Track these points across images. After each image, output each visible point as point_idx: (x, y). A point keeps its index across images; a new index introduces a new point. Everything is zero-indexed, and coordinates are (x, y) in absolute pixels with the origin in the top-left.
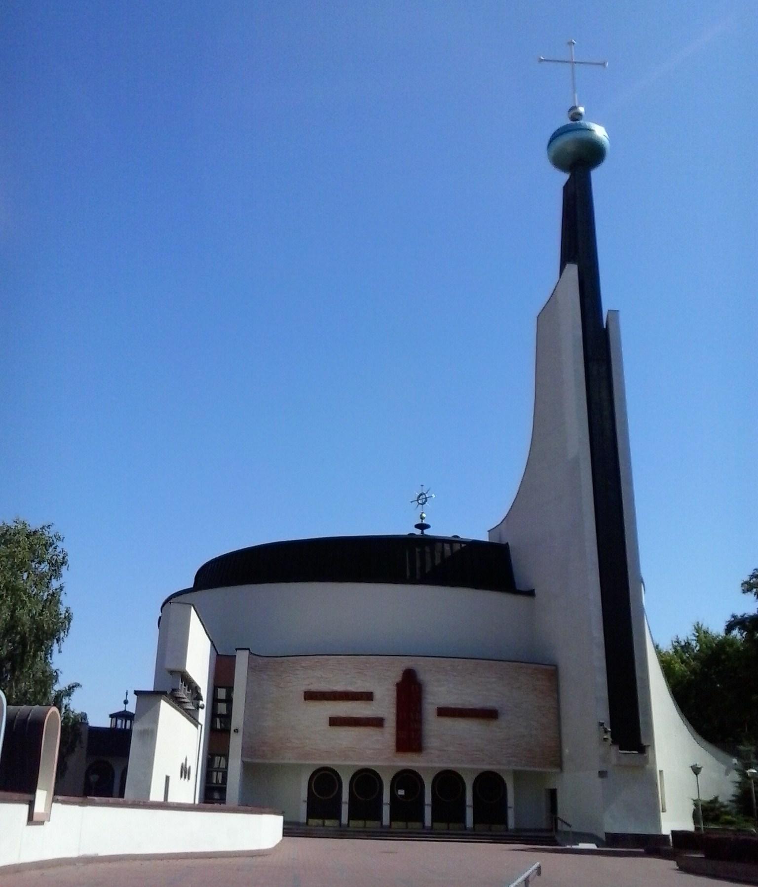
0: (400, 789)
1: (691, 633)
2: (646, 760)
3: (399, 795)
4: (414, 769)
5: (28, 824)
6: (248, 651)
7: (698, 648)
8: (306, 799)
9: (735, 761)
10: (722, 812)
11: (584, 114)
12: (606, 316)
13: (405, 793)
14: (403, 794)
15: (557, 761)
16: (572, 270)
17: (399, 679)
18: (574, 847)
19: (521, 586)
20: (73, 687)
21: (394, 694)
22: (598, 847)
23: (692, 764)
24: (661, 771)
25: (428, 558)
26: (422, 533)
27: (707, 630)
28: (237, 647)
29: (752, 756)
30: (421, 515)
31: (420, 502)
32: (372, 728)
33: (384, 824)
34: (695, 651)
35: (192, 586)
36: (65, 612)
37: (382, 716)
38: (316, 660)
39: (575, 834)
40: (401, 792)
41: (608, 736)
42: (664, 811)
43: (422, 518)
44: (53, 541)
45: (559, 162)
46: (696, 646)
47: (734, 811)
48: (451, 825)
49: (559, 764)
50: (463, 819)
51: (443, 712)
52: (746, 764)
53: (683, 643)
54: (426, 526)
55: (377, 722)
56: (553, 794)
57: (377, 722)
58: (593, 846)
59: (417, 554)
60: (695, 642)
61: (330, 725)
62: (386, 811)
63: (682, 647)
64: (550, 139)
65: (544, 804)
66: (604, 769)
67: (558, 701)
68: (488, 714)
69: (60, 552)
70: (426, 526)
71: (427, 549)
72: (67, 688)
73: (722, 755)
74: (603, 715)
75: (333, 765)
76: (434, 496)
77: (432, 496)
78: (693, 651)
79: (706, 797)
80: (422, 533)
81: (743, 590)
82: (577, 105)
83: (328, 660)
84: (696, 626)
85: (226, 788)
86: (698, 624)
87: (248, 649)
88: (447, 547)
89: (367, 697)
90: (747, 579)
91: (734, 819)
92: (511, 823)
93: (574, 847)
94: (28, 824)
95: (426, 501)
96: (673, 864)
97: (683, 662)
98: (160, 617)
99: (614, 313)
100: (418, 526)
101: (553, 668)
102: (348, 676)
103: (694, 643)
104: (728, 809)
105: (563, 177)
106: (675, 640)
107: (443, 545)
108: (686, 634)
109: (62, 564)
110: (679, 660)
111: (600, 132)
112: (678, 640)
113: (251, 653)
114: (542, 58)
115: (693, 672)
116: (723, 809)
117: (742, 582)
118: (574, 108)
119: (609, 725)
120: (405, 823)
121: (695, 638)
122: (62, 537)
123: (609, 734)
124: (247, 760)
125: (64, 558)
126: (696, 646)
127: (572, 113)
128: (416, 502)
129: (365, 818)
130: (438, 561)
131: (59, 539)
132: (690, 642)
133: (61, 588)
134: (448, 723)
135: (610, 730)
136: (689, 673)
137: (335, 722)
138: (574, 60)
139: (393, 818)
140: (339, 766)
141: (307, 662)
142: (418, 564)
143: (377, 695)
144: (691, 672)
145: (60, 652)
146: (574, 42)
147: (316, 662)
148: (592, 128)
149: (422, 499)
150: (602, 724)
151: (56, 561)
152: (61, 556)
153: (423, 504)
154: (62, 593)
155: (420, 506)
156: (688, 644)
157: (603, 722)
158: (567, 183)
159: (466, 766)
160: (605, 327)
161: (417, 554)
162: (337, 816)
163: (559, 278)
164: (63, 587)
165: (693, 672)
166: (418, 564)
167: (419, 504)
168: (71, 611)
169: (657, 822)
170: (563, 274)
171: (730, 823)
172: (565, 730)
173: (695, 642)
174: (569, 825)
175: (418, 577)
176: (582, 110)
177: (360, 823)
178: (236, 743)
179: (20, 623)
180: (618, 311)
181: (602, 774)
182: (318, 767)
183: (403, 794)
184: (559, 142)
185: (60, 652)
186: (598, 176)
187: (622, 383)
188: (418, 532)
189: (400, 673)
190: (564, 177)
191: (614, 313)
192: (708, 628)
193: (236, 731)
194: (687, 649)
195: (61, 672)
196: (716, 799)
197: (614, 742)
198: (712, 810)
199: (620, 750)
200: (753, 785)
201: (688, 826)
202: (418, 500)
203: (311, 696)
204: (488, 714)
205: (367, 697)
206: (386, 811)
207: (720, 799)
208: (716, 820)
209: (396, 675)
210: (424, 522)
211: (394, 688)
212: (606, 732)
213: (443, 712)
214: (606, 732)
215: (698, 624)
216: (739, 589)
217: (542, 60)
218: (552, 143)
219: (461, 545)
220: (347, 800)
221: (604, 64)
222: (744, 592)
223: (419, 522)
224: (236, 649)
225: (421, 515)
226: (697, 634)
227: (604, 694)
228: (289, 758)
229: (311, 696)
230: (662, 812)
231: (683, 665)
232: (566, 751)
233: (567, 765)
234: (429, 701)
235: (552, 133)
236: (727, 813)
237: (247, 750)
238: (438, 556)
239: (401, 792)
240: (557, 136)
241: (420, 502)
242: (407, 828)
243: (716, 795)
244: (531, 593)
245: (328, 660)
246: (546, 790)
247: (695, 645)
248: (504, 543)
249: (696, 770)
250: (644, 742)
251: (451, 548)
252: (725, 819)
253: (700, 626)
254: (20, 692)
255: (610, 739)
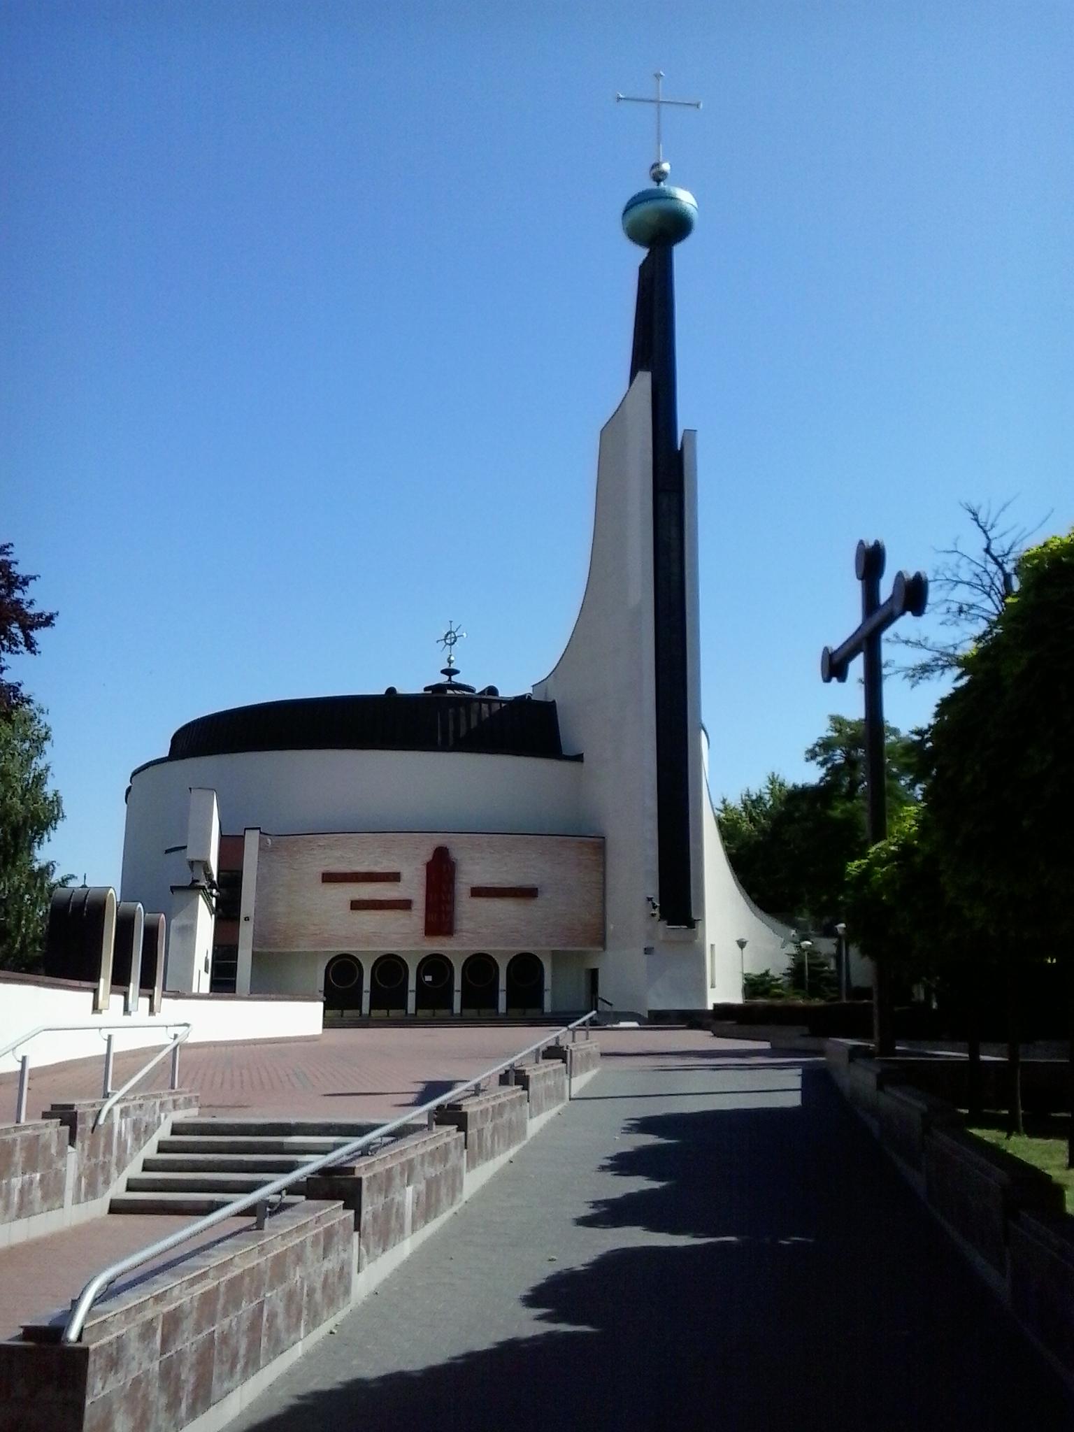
0: (427, 975)
1: (764, 786)
2: (695, 935)
3: (427, 982)
4: (399, 955)
5: (124, 1014)
6: (258, 831)
7: (771, 803)
8: (323, 989)
9: (793, 932)
10: (772, 985)
11: (669, 172)
12: (682, 435)
13: (433, 978)
14: (431, 980)
15: (601, 940)
16: (645, 378)
17: (429, 858)
18: (614, 1026)
19: (566, 751)
20: (67, 879)
21: (424, 873)
22: (640, 1024)
23: (738, 939)
24: (712, 946)
25: (463, 720)
26: (450, 680)
27: (783, 781)
28: (247, 827)
29: (810, 927)
30: (449, 658)
31: (447, 641)
32: (399, 911)
33: (409, 1012)
34: (768, 806)
35: (167, 755)
36: (52, 795)
37: (409, 898)
38: (335, 839)
39: (616, 1013)
40: (428, 978)
41: (656, 912)
42: (713, 986)
43: (450, 662)
44: (35, 714)
45: (636, 234)
46: (769, 801)
47: (785, 985)
48: (482, 1011)
49: (602, 942)
50: (495, 1005)
51: (477, 892)
52: (804, 935)
53: (754, 797)
54: (456, 672)
55: (405, 905)
56: (594, 974)
57: (405, 905)
58: (635, 1024)
59: (451, 716)
60: (769, 795)
61: (351, 909)
62: (411, 998)
63: (753, 802)
64: (628, 203)
65: (584, 979)
66: (650, 945)
67: (604, 874)
68: (527, 893)
69: (42, 727)
70: (456, 672)
71: (462, 710)
72: (60, 880)
73: (779, 926)
74: (653, 890)
75: (488, 951)
76: (464, 634)
77: (462, 636)
78: (765, 806)
79: (757, 971)
80: (450, 680)
81: (807, 759)
82: (661, 161)
83: (351, 838)
84: (771, 778)
85: (235, 981)
86: (773, 774)
87: (259, 828)
88: (485, 707)
89: (394, 877)
90: (810, 747)
91: (783, 992)
92: (547, 1006)
93: (614, 1026)
94: (124, 1014)
95: (455, 641)
96: (710, 1033)
97: (752, 820)
98: (129, 790)
99: (690, 433)
100: (444, 672)
101: (601, 839)
102: (372, 856)
103: (767, 797)
104: (780, 982)
105: (642, 253)
106: (744, 793)
107: (481, 706)
108: (758, 785)
109: (45, 739)
110: (748, 819)
111: (686, 198)
112: (749, 792)
113: (261, 833)
114: (621, 96)
115: (763, 831)
116: (773, 983)
117: (806, 750)
118: (657, 165)
119: (658, 900)
120: (432, 1010)
121: (768, 791)
122: (45, 710)
123: (657, 909)
124: (257, 950)
125: (47, 733)
126: (769, 801)
127: (654, 171)
128: (443, 641)
129: (388, 1007)
130: (474, 723)
131: (42, 711)
132: (762, 795)
133: (47, 768)
134: (483, 903)
135: (658, 905)
136: (757, 833)
137: (357, 905)
138: (661, 100)
139: (418, 1006)
140: (495, 952)
141: (323, 841)
142: (451, 728)
143: (404, 876)
144: (759, 832)
145: (49, 840)
146: (662, 74)
147: (336, 840)
148: (678, 196)
149: (450, 638)
150: (650, 899)
151: (38, 737)
152: (44, 730)
153: (451, 644)
154: (49, 773)
155: (448, 647)
156: (760, 798)
157: (652, 897)
158: (645, 262)
159: (499, 948)
160: (679, 449)
161: (451, 716)
162: (358, 1006)
163: (627, 388)
164: (49, 767)
165: (763, 831)
166: (451, 728)
167: (447, 644)
168: (60, 794)
169: (702, 995)
170: (635, 381)
171: (780, 996)
172: (609, 906)
173: (769, 795)
174: (611, 1005)
175: (451, 742)
176: (666, 167)
177: (383, 1013)
178: (246, 933)
179: (13, 812)
180: (695, 431)
181: (648, 951)
182: (428, 954)
183: (431, 980)
184: (639, 211)
185: (49, 840)
186: (681, 253)
187: (695, 518)
188: (444, 679)
189: (431, 851)
190: (642, 253)
191: (690, 433)
192: (784, 780)
193: (247, 919)
194: (758, 803)
195: (59, 865)
196: (766, 974)
197: (662, 918)
198: (762, 983)
199: (668, 925)
200: (806, 958)
201: (737, 998)
202: (445, 640)
203: (329, 878)
204: (527, 893)
205: (394, 877)
206: (411, 998)
207: (771, 973)
208: (765, 993)
209: (426, 855)
210: (453, 666)
211: (424, 868)
212: (654, 907)
213: (477, 892)
214: (654, 907)
215: (773, 774)
216: (803, 756)
217: (622, 99)
218: (628, 211)
219: (501, 705)
220: (369, 989)
221: (698, 106)
222: (807, 760)
223: (446, 666)
224: (246, 829)
225: (449, 658)
226: (771, 786)
227: (655, 867)
228: (304, 946)
229: (329, 878)
230: (712, 987)
231: (751, 825)
232: (611, 927)
233: (610, 942)
234: (461, 880)
235: (630, 197)
236: (778, 987)
237: (258, 939)
238: (474, 719)
239: (428, 978)
240: (636, 204)
241: (447, 641)
242: (434, 1015)
243: (768, 969)
244: (579, 758)
245: (351, 838)
246: (587, 969)
247: (768, 799)
248: (551, 701)
249: (742, 944)
250: (694, 916)
251: (490, 708)
252: (776, 992)
253: (775, 777)
254: (13, 887)
255: (658, 915)
